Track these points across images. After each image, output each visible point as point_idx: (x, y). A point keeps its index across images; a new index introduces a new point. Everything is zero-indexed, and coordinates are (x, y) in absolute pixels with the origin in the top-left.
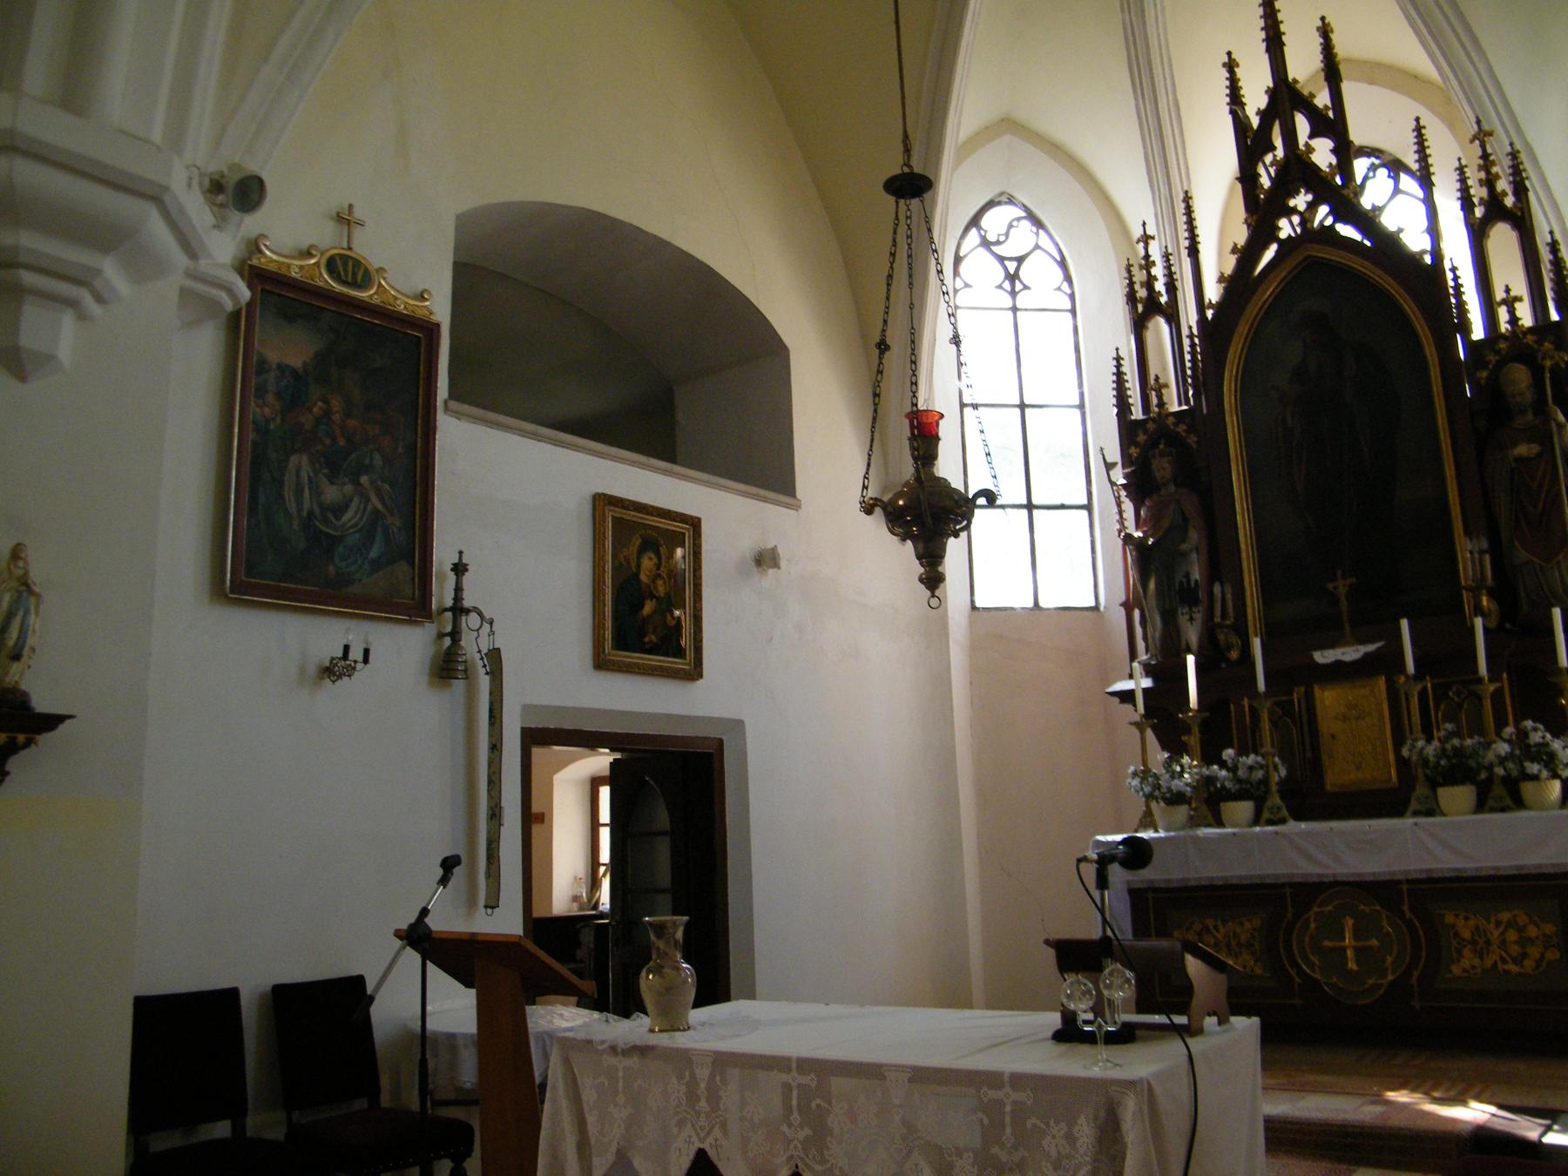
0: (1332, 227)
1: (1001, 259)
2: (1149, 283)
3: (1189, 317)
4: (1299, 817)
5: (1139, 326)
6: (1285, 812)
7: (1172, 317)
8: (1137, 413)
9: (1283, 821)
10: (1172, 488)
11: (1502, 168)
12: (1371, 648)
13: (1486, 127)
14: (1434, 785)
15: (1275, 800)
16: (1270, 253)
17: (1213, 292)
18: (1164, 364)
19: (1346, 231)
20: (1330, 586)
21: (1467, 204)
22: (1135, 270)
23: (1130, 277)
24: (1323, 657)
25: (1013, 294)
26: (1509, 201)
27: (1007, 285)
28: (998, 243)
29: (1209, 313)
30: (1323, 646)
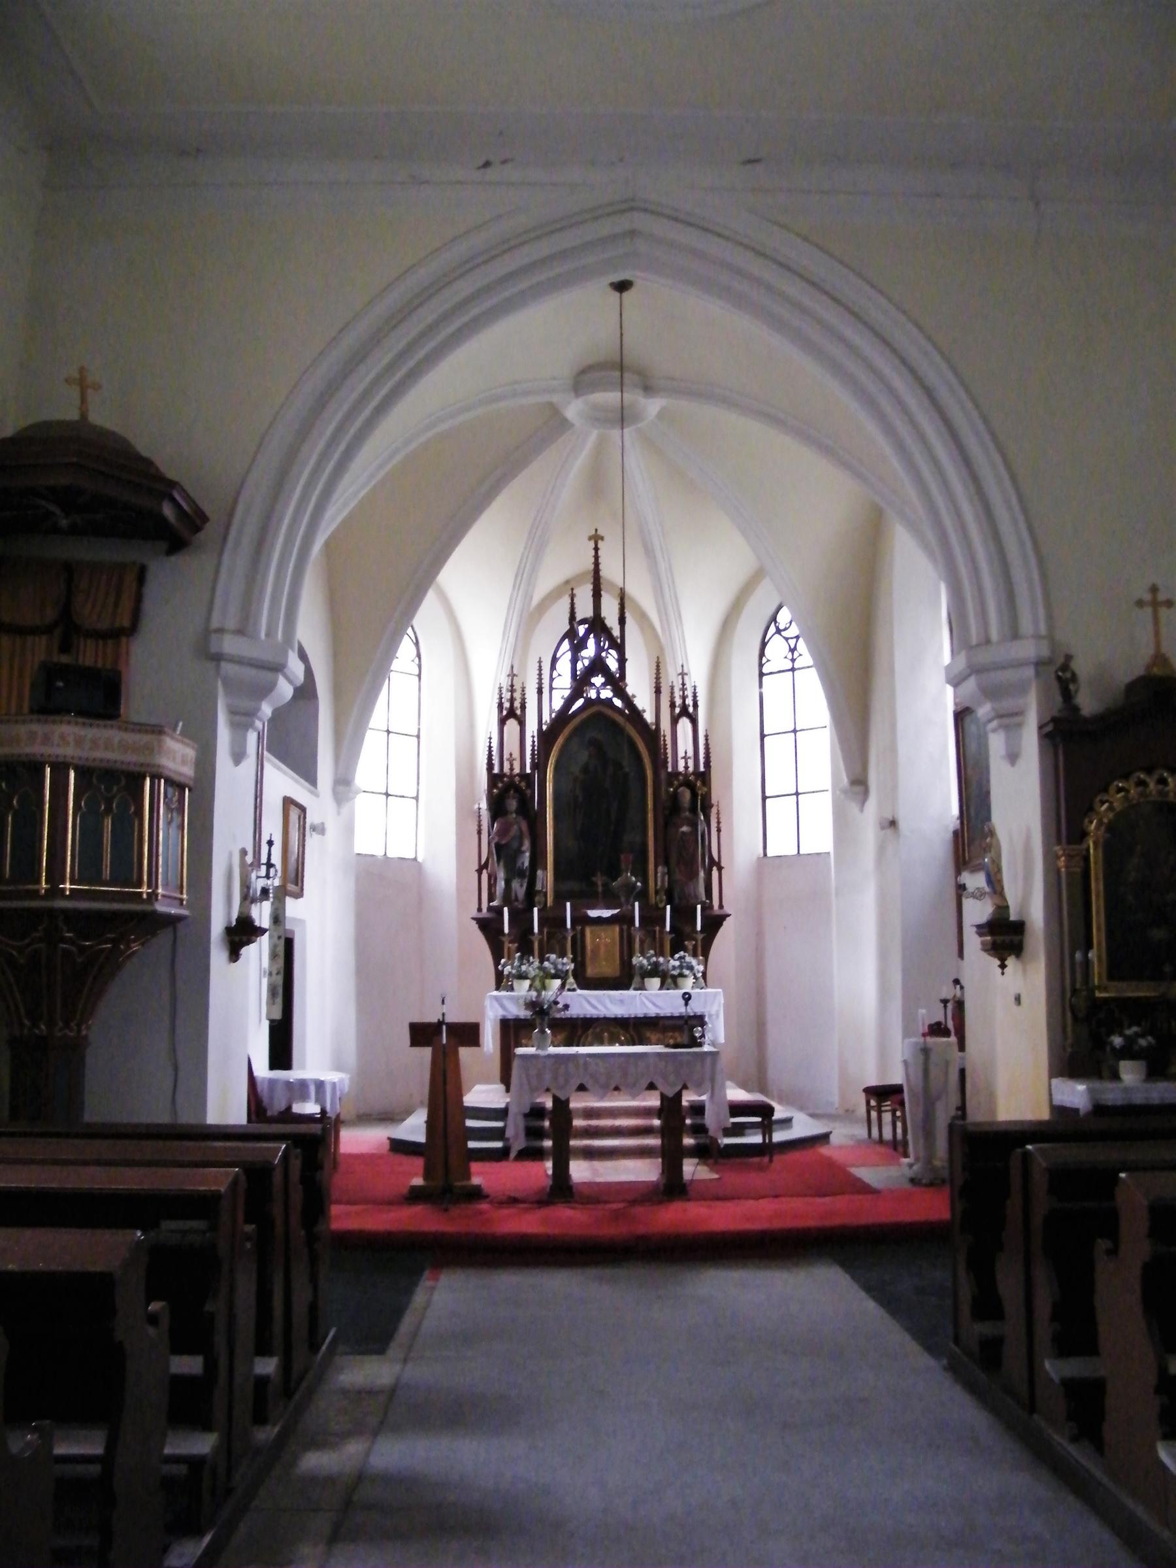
0: (611, 699)
1: (787, 639)
2: (512, 700)
3: (532, 727)
4: (582, 988)
5: (502, 722)
6: (575, 986)
7: (522, 723)
8: (496, 770)
9: (574, 990)
10: (514, 815)
11: (689, 693)
12: (616, 911)
13: (686, 671)
14: (643, 978)
15: (571, 980)
16: (580, 703)
17: (546, 718)
18: (512, 746)
19: (618, 703)
20: (145, 896)
21: (673, 705)
22: (504, 691)
23: (501, 695)
24: (593, 913)
25: (793, 660)
26: (691, 710)
27: (790, 656)
28: (786, 629)
29: (544, 727)
30: (593, 908)
